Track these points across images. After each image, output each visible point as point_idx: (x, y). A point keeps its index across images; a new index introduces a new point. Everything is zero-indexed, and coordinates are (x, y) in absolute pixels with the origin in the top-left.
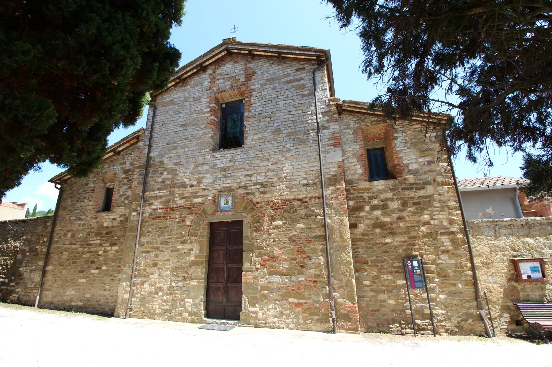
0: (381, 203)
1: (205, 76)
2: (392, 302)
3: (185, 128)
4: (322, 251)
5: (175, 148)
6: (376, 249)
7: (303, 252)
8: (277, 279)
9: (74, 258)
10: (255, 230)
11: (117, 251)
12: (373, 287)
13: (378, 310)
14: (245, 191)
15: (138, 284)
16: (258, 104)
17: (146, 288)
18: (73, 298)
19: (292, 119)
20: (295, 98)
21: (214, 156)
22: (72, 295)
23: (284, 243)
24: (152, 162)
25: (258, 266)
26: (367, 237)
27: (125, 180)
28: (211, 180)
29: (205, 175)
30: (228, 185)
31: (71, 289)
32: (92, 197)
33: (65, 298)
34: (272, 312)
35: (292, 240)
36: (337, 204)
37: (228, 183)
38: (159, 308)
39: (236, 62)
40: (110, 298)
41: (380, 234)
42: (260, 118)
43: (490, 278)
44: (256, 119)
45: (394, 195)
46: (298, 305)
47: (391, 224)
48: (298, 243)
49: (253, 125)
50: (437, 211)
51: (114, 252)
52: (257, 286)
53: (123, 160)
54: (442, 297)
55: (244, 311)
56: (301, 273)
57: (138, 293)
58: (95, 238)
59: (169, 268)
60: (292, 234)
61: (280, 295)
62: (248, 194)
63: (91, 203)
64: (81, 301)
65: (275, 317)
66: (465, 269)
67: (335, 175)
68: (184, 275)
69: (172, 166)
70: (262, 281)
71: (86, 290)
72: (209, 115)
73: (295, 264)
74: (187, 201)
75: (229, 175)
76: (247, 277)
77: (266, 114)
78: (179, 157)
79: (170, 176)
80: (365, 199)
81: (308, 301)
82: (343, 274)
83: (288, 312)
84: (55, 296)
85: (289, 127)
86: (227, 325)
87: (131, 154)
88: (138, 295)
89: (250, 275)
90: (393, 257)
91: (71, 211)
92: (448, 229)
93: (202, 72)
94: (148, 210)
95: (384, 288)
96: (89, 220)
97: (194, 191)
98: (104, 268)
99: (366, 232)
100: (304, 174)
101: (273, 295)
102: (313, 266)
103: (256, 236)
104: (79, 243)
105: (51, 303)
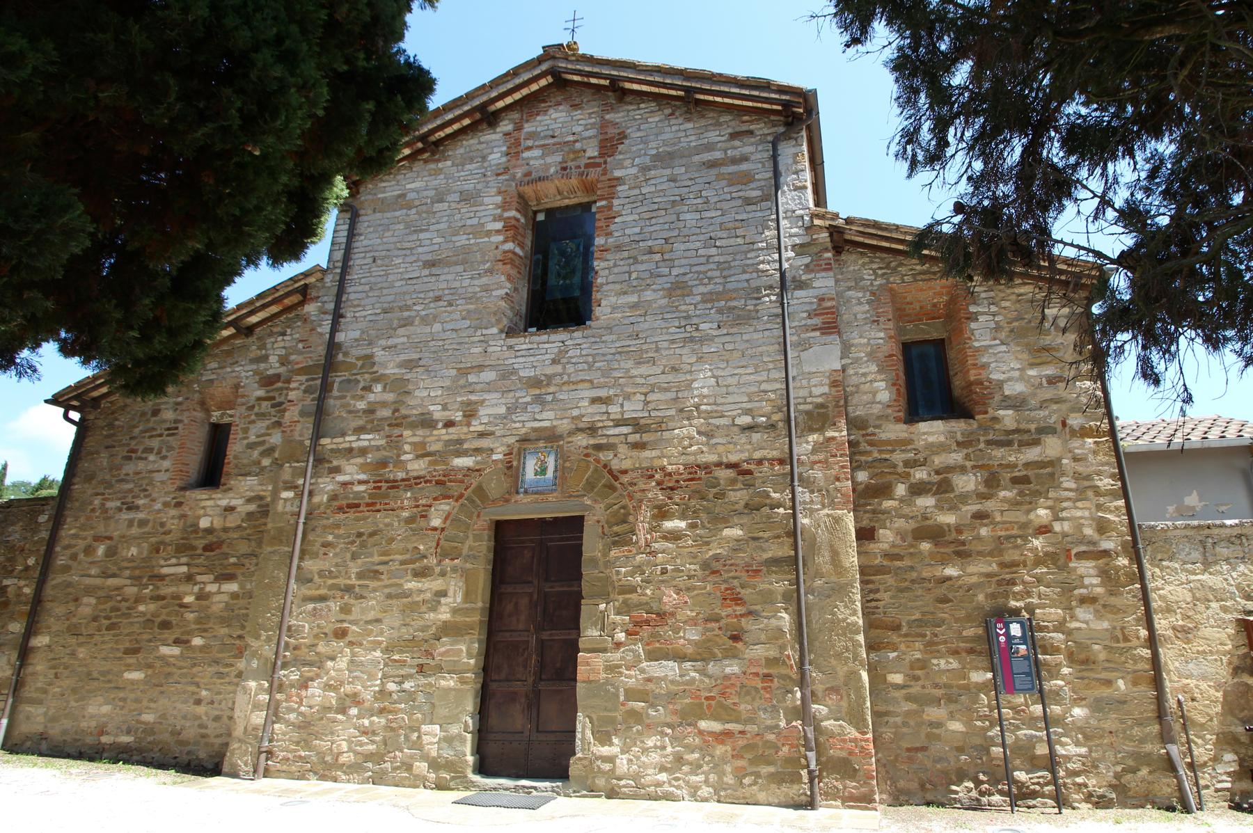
0: (936, 478)
1: (493, 137)
2: (956, 726)
3: (434, 271)
4: (786, 597)
5: (407, 323)
6: (920, 592)
7: (738, 600)
8: (670, 669)
9: (113, 615)
10: (615, 543)
11: (235, 596)
13: (924, 749)
14: (592, 442)
15: (292, 686)
17: (313, 696)
18: (105, 725)
19: (716, 259)
20: (725, 206)
21: (511, 347)
22: (104, 715)
23: (690, 577)
24: (340, 357)
25: (621, 636)
26: (898, 564)
27: (265, 404)
28: (503, 410)
29: (486, 396)
31: (100, 699)
32: (170, 448)
33: (84, 724)
34: (655, 757)
35: (710, 568)
37: (547, 419)
38: (350, 750)
39: (575, 106)
41: (931, 554)
43: (1191, 666)
44: (626, 254)
45: (967, 457)
47: (959, 532)
48: (725, 576)
49: (616, 270)
50: (1069, 499)
51: (225, 598)
52: (617, 689)
54: (1078, 712)
55: (579, 755)
56: (731, 654)
57: (290, 710)
58: (174, 561)
59: (380, 643)
60: (711, 553)
61: (675, 712)
62: (599, 447)
63: (166, 464)
64: (128, 732)
65: (663, 769)
66: (1135, 642)
67: (822, 406)
68: (420, 661)
69: (396, 371)
70: (629, 677)
71: (145, 703)
72: (501, 238)
73: (717, 632)
76: (590, 665)
77: (650, 243)
79: (390, 397)
80: (895, 466)
82: (838, 656)
83: (697, 755)
84: (54, 719)
85: (710, 279)
86: (535, 793)
87: (284, 334)
88: (292, 716)
89: (598, 661)
90: (962, 614)
94: (327, 485)
95: (938, 692)
96: (159, 511)
97: (455, 437)
98: (197, 641)
99: (896, 551)
100: (746, 399)
101: (658, 713)
102: (763, 637)
104: (127, 573)
105: (43, 737)
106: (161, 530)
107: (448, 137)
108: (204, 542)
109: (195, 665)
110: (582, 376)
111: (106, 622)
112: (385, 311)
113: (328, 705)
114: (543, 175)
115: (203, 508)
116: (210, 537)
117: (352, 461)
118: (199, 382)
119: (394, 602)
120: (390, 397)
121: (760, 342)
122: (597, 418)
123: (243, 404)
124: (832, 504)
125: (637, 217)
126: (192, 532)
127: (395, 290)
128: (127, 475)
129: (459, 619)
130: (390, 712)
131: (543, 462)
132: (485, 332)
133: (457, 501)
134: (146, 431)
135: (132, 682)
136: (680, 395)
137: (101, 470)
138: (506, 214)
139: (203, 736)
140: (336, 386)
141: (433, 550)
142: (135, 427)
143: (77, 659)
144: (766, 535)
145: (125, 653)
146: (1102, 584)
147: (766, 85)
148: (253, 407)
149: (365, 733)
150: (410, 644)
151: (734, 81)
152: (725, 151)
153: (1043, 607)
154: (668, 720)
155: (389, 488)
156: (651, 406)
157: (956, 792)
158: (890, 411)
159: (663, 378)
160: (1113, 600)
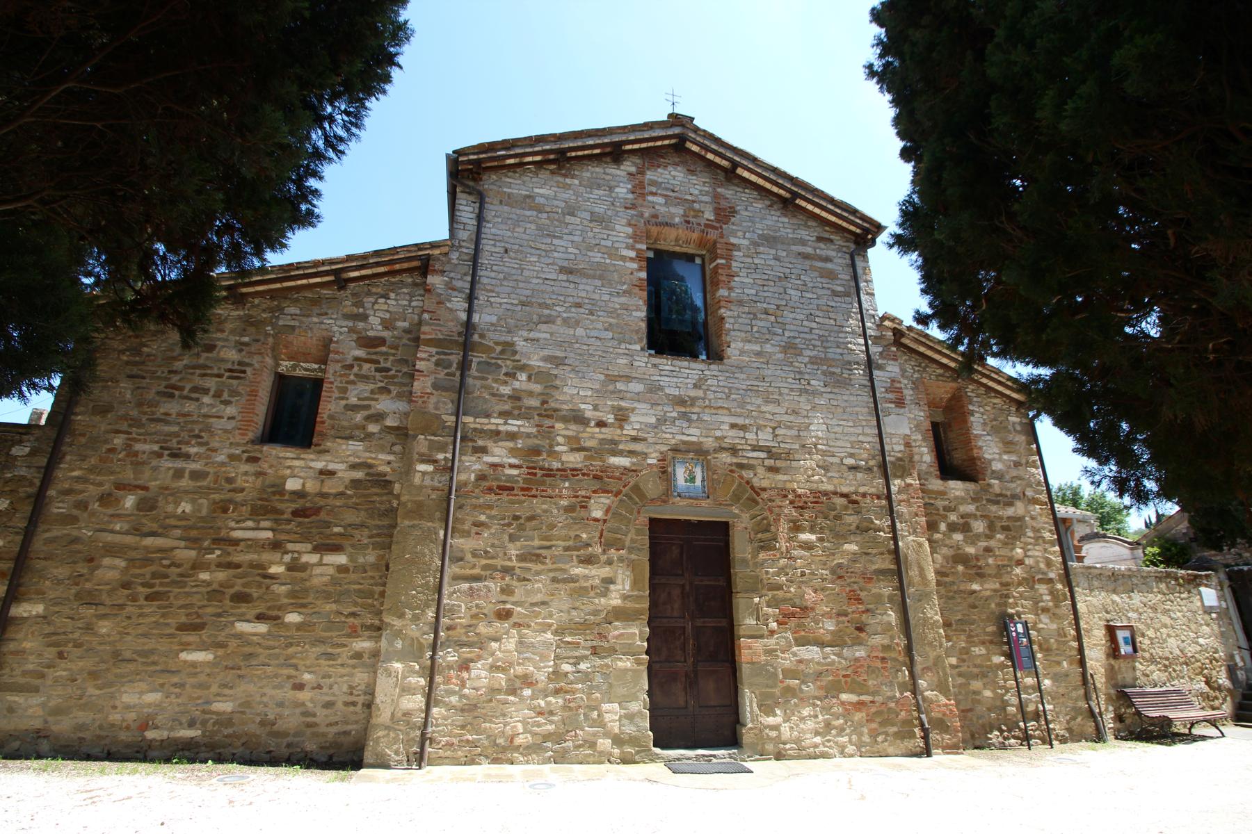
0: (961, 521)
1: (618, 172)
3: (571, 278)
5: (549, 320)
8: (812, 653)
9: (155, 584)
10: (761, 547)
11: (342, 569)
14: (735, 460)
18: (150, 717)
20: (820, 292)
21: (655, 366)
22: (149, 705)
23: (823, 580)
24: (476, 337)
25: (774, 625)
26: (946, 579)
27: (366, 366)
28: (653, 420)
29: (635, 405)
30: (694, 439)
31: (143, 686)
32: (234, 393)
33: (115, 717)
34: (810, 724)
35: (838, 573)
36: (910, 513)
37: (694, 434)
38: (525, 731)
39: (692, 172)
40: (321, 713)
44: (746, 309)
45: (977, 509)
47: (978, 560)
51: (331, 571)
52: (776, 669)
53: (355, 305)
55: (750, 725)
56: (858, 642)
59: (550, 625)
61: (821, 688)
62: (741, 466)
63: (230, 410)
64: (191, 724)
65: (817, 733)
66: (1069, 638)
67: (900, 459)
68: (594, 643)
69: (541, 364)
70: (785, 659)
72: (635, 266)
75: (695, 417)
76: (750, 650)
77: (765, 305)
78: (560, 344)
79: (537, 388)
81: (877, 698)
82: (930, 644)
83: (841, 721)
84: (57, 711)
86: (715, 761)
87: (386, 297)
88: (454, 699)
89: (758, 645)
91: (136, 423)
93: (608, 159)
94: (470, 467)
95: (976, 670)
96: (223, 464)
97: (609, 437)
98: (293, 618)
101: (810, 689)
102: (879, 629)
103: (765, 561)
104: (178, 532)
105: (40, 735)
106: (228, 486)
107: (577, 158)
108: (294, 506)
109: (291, 645)
112: (523, 304)
113: (497, 686)
115: (289, 467)
117: (500, 444)
118: (274, 326)
119: (560, 586)
122: (737, 441)
123: (338, 361)
124: (915, 532)
126: (274, 493)
128: (167, 414)
129: (629, 604)
130: (566, 692)
131: (691, 473)
133: (616, 496)
134: (194, 367)
135: (194, 665)
139: (309, 725)
140: (474, 365)
143: (96, 634)
144: (874, 551)
145: (178, 629)
146: (1051, 600)
148: (351, 367)
149: (540, 714)
151: (832, 200)
152: (815, 249)
153: (1024, 613)
156: (780, 439)
159: (786, 418)
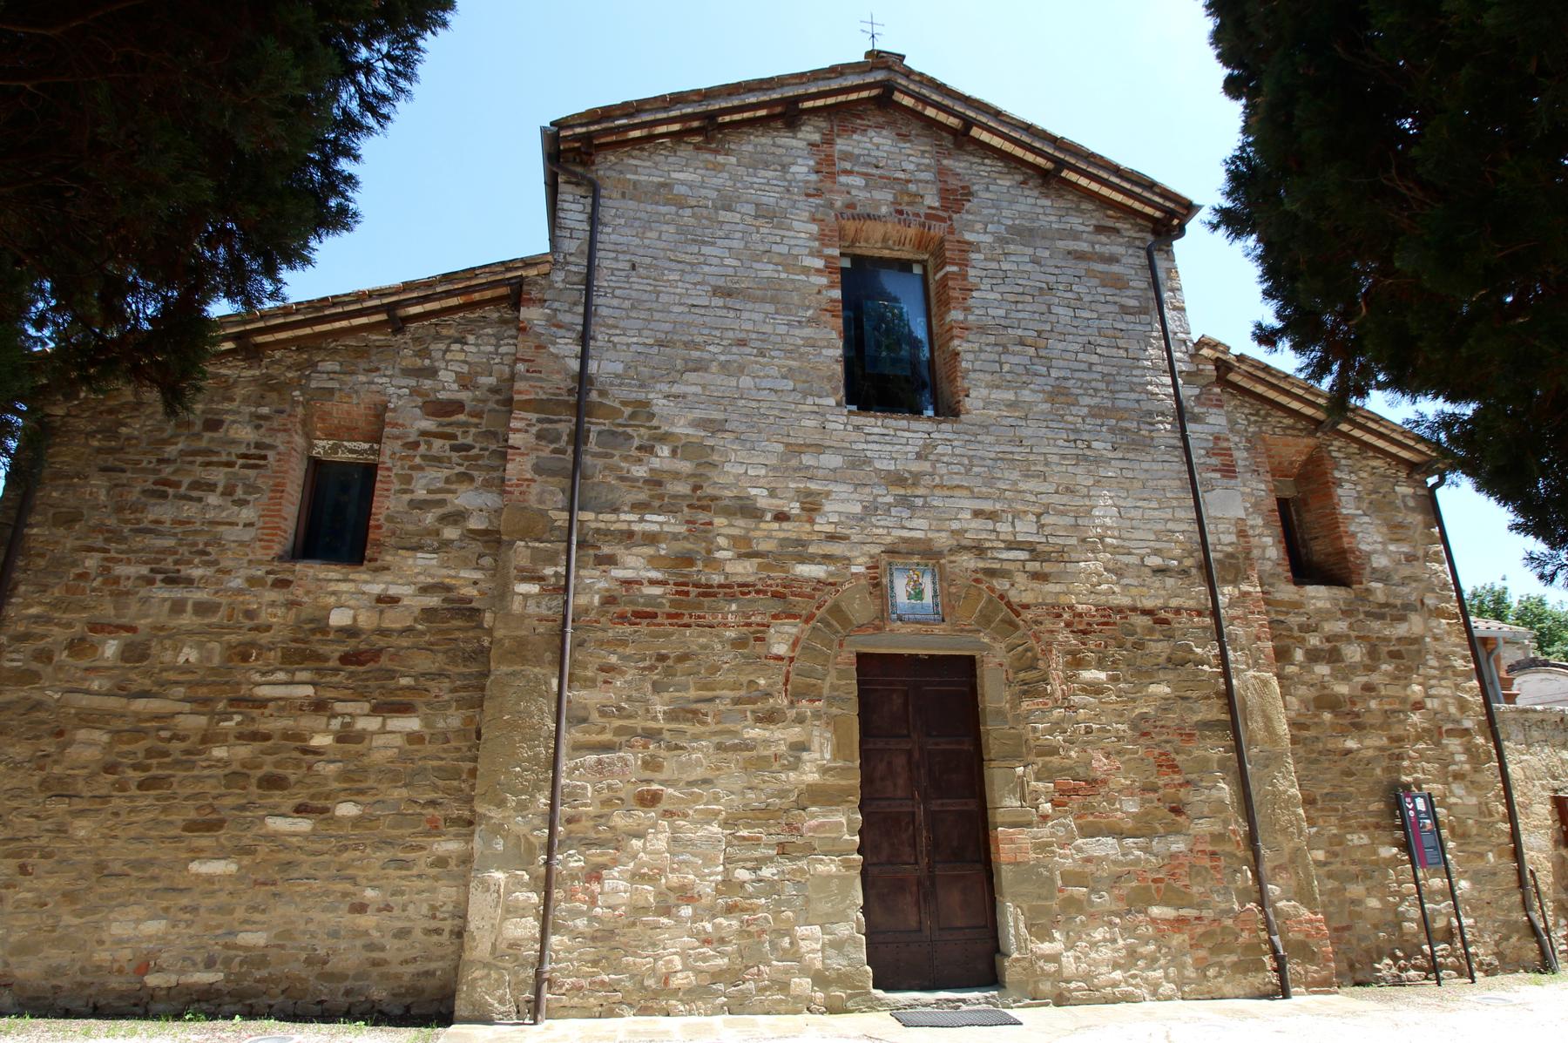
0: (1327, 646)
1: (794, 142)
2: (1374, 903)
3: (730, 302)
4: (1222, 766)
5: (700, 367)
6: (1326, 765)
7: (1174, 767)
8: (1105, 847)
9: (151, 764)
10: (1025, 693)
12: (1333, 867)
13: (1348, 928)
14: (981, 565)
15: (573, 877)
16: (991, 296)
17: (615, 891)
19: (1099, 368)
20: (1102, 309)
21: (857, 428)
22: (149, 938)
25: (1047, 807)
26: (1306, 733)
27: (438, 443)
28: (857, 509)
29: (831, 487)
30: (919, 535)
31: (139, 911)
32: (251, 488)
33: (102, 956)
34: (1106, 953)
37: (919, 528)
38: (686, 968)
39: (903, 137)
40: (392, 944)
41: (1333, 725)
42: (1005, 341)
44: (992, 339)
45: (1351, 626)
46: (1179, 924)
47: (1354, 704)
48: (1158, 739)
49: (983, 356)
50: (1434, 677)
51: (399, 741)
52: (1052, 873)
53: (418, 354)
55: (1015, 955)
56: (1173, 830)
57: (578, 914)
58: (281, 676)
60: (1137, 711)
62: (992, 573)
63: (247, 514)
64: (210, 964)
65: (1116, 966)
67: (1231, 556)
68: (782, 838)
69: (690, 431)
70: (1065, 857)
71: (240, 913)
72: (824, 281)
73: (1156, 804)
74: (768, 567)
75: (919, 502)
76: (1013, 845)
77: (1020, 332)
78: (717, 401)
79: (686, 467)
80: (1291, 630)
81: (1204, 913)
82: (1284, 830)
85: (1096, 390)
86: (964, 1007)
88: (581, 923)
89: (1024, 837)
90: (1365, 788)
91: (115, 536)
92: (1458, 722)
94: (592, 585)
95: (1354, 869)
96: (240, 591)
97: (794, 536)
98: (347, 810)
99: (1302, 720)
100: (1153, 537)
101: (1103, 900)
102: (1206, 810)
103: (1031, 712)
104: (180, 691)
107: (1075, 185)
109: (346, 848)
110: (957, 481)
111: (135, 776)
113: (642, 903)
114: (872, 212)
115: (334, 593)
116: (353, 642)
117: (635, 550)
119: (729, 755)
120: (686, 467)
121: (1160, 474)
125: (999, 297)
126: (313, 631)
127: (672, 316)
128: (157, 522)
129: (830, 780)
130: (743, 910)
131: (917, 584)
132: (818, 401)
133: (806, 622)
135: (210, 879)
136: (1080, 522)
137: (95, 507)
138: (828, 251)
141: (780, 686)
142: (166, 442)
143: (70, 839)
145: (185, 829)
147: (1151, 185)
148: (416, 445)
150: (763, 815)
151: (1116, 170)
154: (1114, 908)
155: (699, 595)
156: (1047, 530)
157: (1379, 970)
158: (1280, 569)
159: (1056, 499)
160: (1477, 777)
